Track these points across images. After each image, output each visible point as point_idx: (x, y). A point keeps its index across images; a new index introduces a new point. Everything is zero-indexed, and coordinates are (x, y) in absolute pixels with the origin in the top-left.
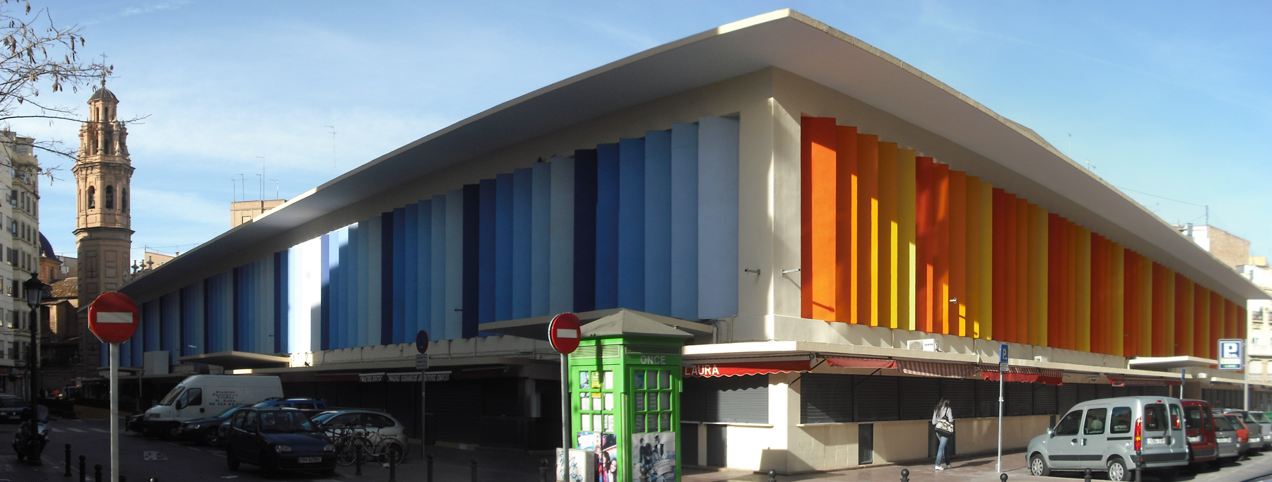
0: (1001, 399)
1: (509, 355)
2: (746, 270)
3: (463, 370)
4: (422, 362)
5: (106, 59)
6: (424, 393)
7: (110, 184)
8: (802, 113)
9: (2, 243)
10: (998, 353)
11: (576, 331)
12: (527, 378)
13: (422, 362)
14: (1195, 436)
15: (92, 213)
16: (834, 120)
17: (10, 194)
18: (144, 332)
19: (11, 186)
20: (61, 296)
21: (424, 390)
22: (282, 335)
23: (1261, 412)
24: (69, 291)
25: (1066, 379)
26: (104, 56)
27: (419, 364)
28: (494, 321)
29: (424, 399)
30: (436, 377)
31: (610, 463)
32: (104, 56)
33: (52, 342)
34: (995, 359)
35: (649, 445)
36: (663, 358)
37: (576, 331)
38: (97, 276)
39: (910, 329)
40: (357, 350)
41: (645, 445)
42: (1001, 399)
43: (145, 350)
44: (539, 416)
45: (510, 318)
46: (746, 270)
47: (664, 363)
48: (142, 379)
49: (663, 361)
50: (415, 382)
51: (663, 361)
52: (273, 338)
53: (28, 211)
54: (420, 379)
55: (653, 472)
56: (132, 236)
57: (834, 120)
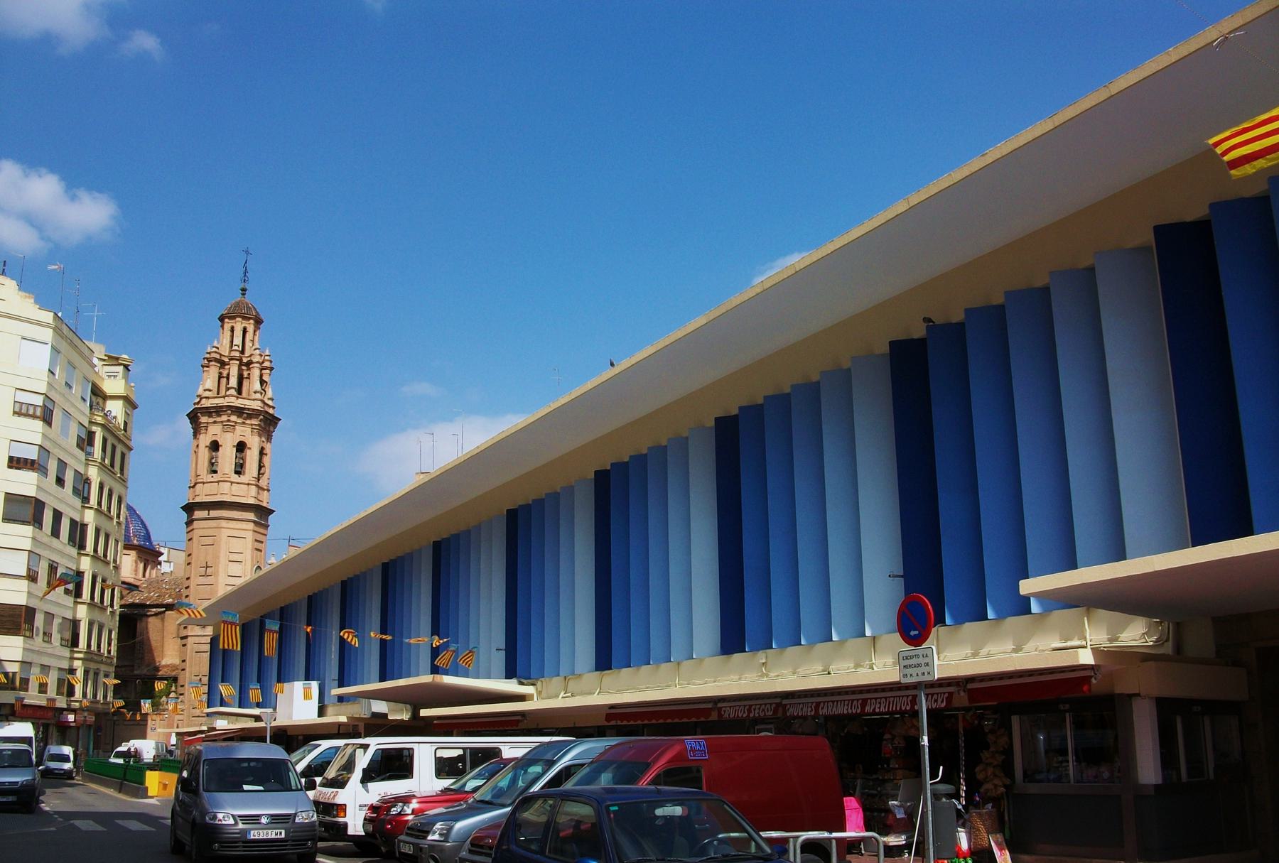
3: (970, 686)
4: (919, 665)
6: (926, 738)
7: (242, 439)
12: (1138, 695)
13: (919, 665)
15: (212, 480)
27: (908, 671)
29: (927, 750)
44: (1160, 782)
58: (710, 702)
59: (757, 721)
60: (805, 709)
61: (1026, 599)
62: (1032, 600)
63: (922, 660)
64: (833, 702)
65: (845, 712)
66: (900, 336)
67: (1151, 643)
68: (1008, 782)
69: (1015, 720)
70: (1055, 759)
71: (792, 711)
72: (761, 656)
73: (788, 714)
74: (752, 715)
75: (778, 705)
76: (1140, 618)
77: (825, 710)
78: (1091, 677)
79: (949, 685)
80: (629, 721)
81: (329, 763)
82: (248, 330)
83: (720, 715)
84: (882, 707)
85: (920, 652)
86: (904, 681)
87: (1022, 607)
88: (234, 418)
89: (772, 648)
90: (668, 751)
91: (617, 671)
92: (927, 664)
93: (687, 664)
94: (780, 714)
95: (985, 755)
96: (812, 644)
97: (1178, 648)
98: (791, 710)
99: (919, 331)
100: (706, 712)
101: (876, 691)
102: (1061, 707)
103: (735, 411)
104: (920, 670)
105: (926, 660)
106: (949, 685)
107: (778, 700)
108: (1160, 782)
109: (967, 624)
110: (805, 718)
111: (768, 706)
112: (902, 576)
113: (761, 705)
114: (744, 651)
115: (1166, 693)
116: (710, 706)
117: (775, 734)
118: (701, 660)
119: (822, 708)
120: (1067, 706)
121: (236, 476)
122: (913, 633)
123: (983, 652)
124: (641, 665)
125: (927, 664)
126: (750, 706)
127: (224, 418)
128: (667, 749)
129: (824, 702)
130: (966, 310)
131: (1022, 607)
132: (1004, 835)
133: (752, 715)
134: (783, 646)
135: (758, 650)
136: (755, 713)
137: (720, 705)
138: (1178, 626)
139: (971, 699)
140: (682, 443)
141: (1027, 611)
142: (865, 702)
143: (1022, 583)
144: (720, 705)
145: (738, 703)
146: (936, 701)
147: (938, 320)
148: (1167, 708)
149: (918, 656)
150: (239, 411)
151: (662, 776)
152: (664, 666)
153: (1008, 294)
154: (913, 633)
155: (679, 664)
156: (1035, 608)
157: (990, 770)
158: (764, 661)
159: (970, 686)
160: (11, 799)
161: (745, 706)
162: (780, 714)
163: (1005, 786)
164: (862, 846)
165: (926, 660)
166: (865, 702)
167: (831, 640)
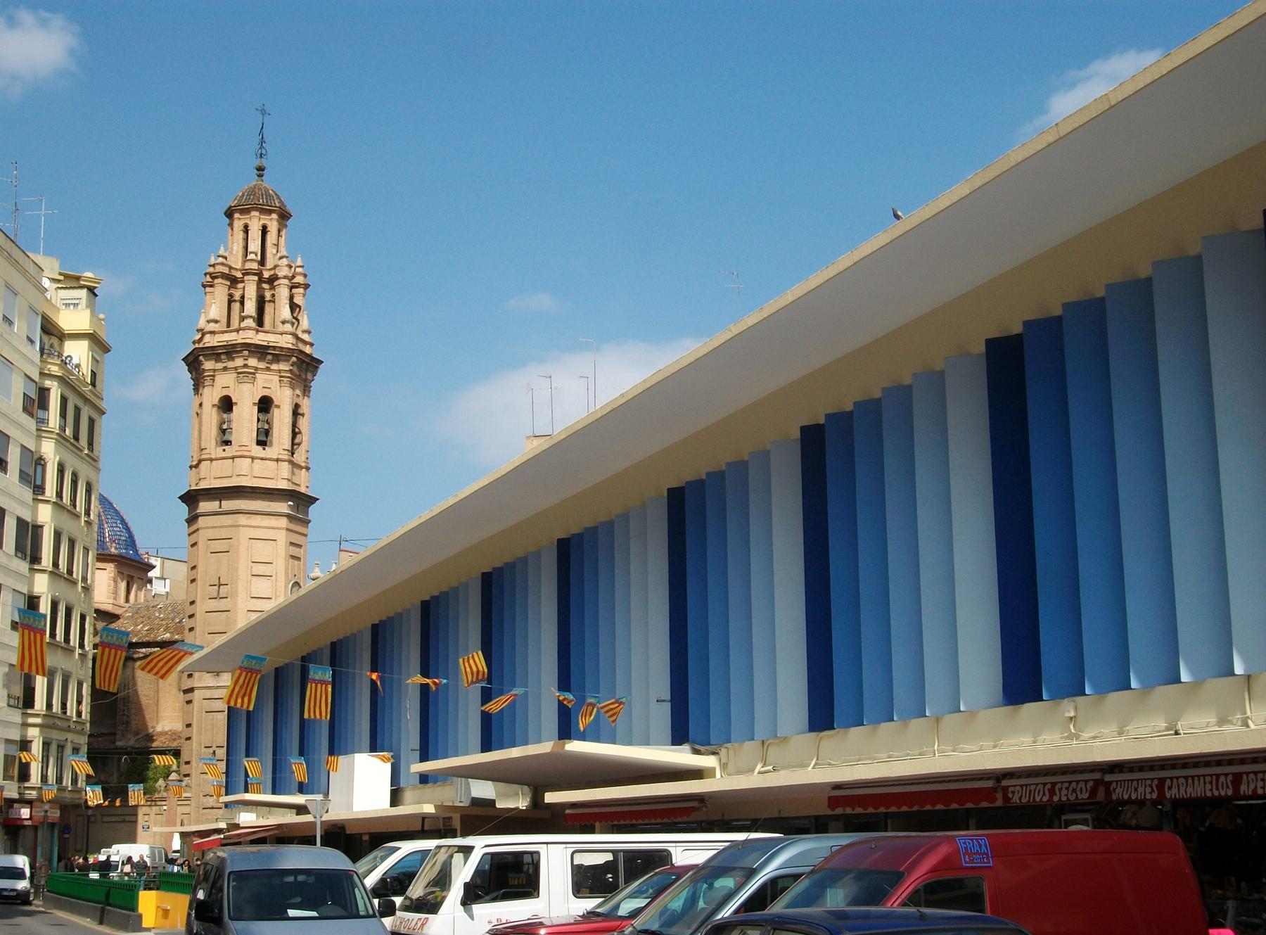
1: (420, 874)
5: (267, 118)
7: (266, 393)
9: (1, 582)
15: (224, 454)
17: (33, 394)
18: (275, 754)
19: (36, 377)
20: (150, 638)
22: (369, 816)
23: (1234, 884)
24: (166, 630)
26: (263, 112)
30: (1052, 792)
32: (263, 112)
33: (119, 744)
38: (232, 595)
39: (612, 859)
43: (332, 751)
48: (322, 822)
52: (667, 706)
53: (76, 438)
56: (312, 508)
59: (1062, 808)
60: (1141, 790)
64: (1186, 778)
71: (1119, 793)
72: (1068, 708)
73: (1114, 797)
74: (1056, 799)
75: (1097, 783)
77: (1174, 791)
82: (269, 229)
83: (1006, 798)
88: (253, 362)
93: (950, 720)
94: (1101, 796)
96: (1147, 687)
107: (1097, 776)
110: (1141, 803)
111: (1082, 785)
113: (1070, 782)
114: (1039, 698)
116: (990, 784)
117: (1094, 827)
118: (972, 714)
121: (260, 448)
126: (1054, 784)
127: (239, 362)
133: (1056, 799)
136: (1062, 796)
142: (1237, 778)
144: (1005, 783)
150: (261, 351)
155: (938, 720)
161: (1045, 784)
162: (1101, 796)
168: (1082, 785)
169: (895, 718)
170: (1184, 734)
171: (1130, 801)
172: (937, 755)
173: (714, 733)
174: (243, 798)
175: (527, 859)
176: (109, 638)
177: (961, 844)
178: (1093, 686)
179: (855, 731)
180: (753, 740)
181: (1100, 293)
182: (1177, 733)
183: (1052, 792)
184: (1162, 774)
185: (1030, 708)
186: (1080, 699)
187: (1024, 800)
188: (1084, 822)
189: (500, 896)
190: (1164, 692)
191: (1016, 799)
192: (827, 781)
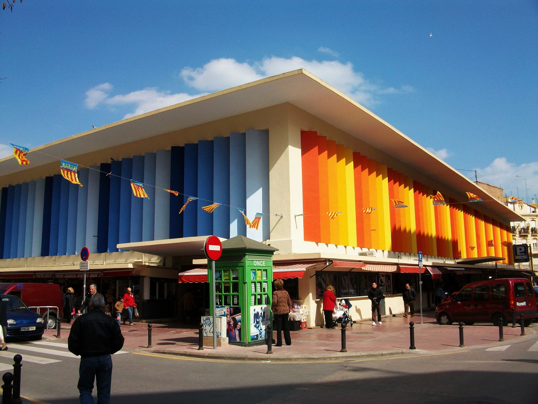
0: (85, 286)
2: (276, 215)
3: (104, 272)
4: (84, 266)
6: (85, 285)
8: (301, 129)
10: (239, 264)
11: (219, 246)
12: (145, 276)
13: (84, 266)
14: (523, 302)
16: (316, 132)
21: (85, 284)
25: (458, 273)
27: (82, 267)
28: (142, 241)
29: (85, 289)
30: (45, 276)
31: (237, 324)
34: (417, 262)
35: (258, 313)
36: (264, 262)
37: (219, 246)
40: (341, 247)
41: (256, 313)
42: (85, 286)
44: (149, 299)
45: (153, 239)
46: (276, 215)
47: (265, 265)
49: (264, 264)
50: (74, 278)
51: (264, 264)
54: (100, 276)
55: (260, 329)
57: (316, 132)
58: (33, 272)
59: (48, 279)
60: (61, 276)
61: (118, 249)
62: (119, 249)
63: (85, 265)
64: (69, 274)
65: (72, 277)
66: (104, 162)
67: (158, 262)
68: (114, 298)
69: (118, 282)
70: (366, 291)
71: (57, 276)
72: (54, 258)
73: (56, 277)
74: (45, 277)
75: (53, 274)
76: (157, 256)
77: (66, 276)
78: (132, 271)
79: (99, 271)
80: (6, 278)
81: (258, 130)
83: (36, 277)
84: (81, 277)
85: (85, 263)
86: (81, 270)
87: (117, 250)
89: (57, 255)
90: (12, 287)
91: (5, 260)
92: (86, 266)
93: (29, 259)
94: (53, 277)
95: (108, 291)
96: (70, 255)
97: (164, 264)
98: (57, 276)
99: (110, 162)
100: (31, 276)
101: (97, 271)
102: (128, 278)
103: (53, 176)
104: (85, 267)
105: (86, 265)
106: (99, 271)
107: (53, 273)
108: (149, 299)
109: (114, 252)
110: (61, 278)
111: (50, 275)
112: (97, 236)
113: (48, 274)
114: (48, 256)
115: (152, 276)
116: (33, 273)
117: (53, 283)
118: (35, 258)
119: (66, 276)
120: (130, 278)
122: (84, 257)
123: (117, 261)
124: (14, 258)
125: (86, 266)
126: (45, 274)
128: (11, 287)
129: (66, 274)
130: (123, 158)
131: (117, 250)
132: (111, 313)
133: (45, 277)
134: (61, 255)
135: (53, 256)
136: (47, 277)
137: (36, 274)
138: (165, 258)
139: (104, 275)
140: (34, 183)
141: (118, 251)
142: (77, 274)
143: (118, 245)
144: (36, 274)
145: (42, 273)
146: (95, 275)
147: (115, 159)
148: (153, 281)
149: (84, 264)
151: (293, 300)
152: (22, 259)
153: (134, 156)
154: (84, 257)
155: (27, 258)
156: (119, 251)
157: (109, 295)
158: (54, 259)
159: (104, 272)
160: (464, 269)
161: (43, 274)
162: (53, 277)
163: (113, 299)
164: (74, 317)
165: (86, 265)
166: (77, 274)
167: (75, 254)
168: (50, 275)
169: (58, 255)
170: (76, 265)
171: (60, 278)
172: (104, 263)
173: (26, 255)
174: (89, 253)
175: (217, 284)
176: (72, 168)
177: (473, 287)
178: (109, 250)
179: (8, 260)
180: (24, 257)
181: (132, 157)
182: (74, 265)
183: (45, 276)
184: (45, 273)
185: (103, 254)
186: (56, 256)
187: (39, 277)
188: (51, 282)
189: (341, 303)
190: (72, 256)
191: (38, 277)
192: (33, 270)
